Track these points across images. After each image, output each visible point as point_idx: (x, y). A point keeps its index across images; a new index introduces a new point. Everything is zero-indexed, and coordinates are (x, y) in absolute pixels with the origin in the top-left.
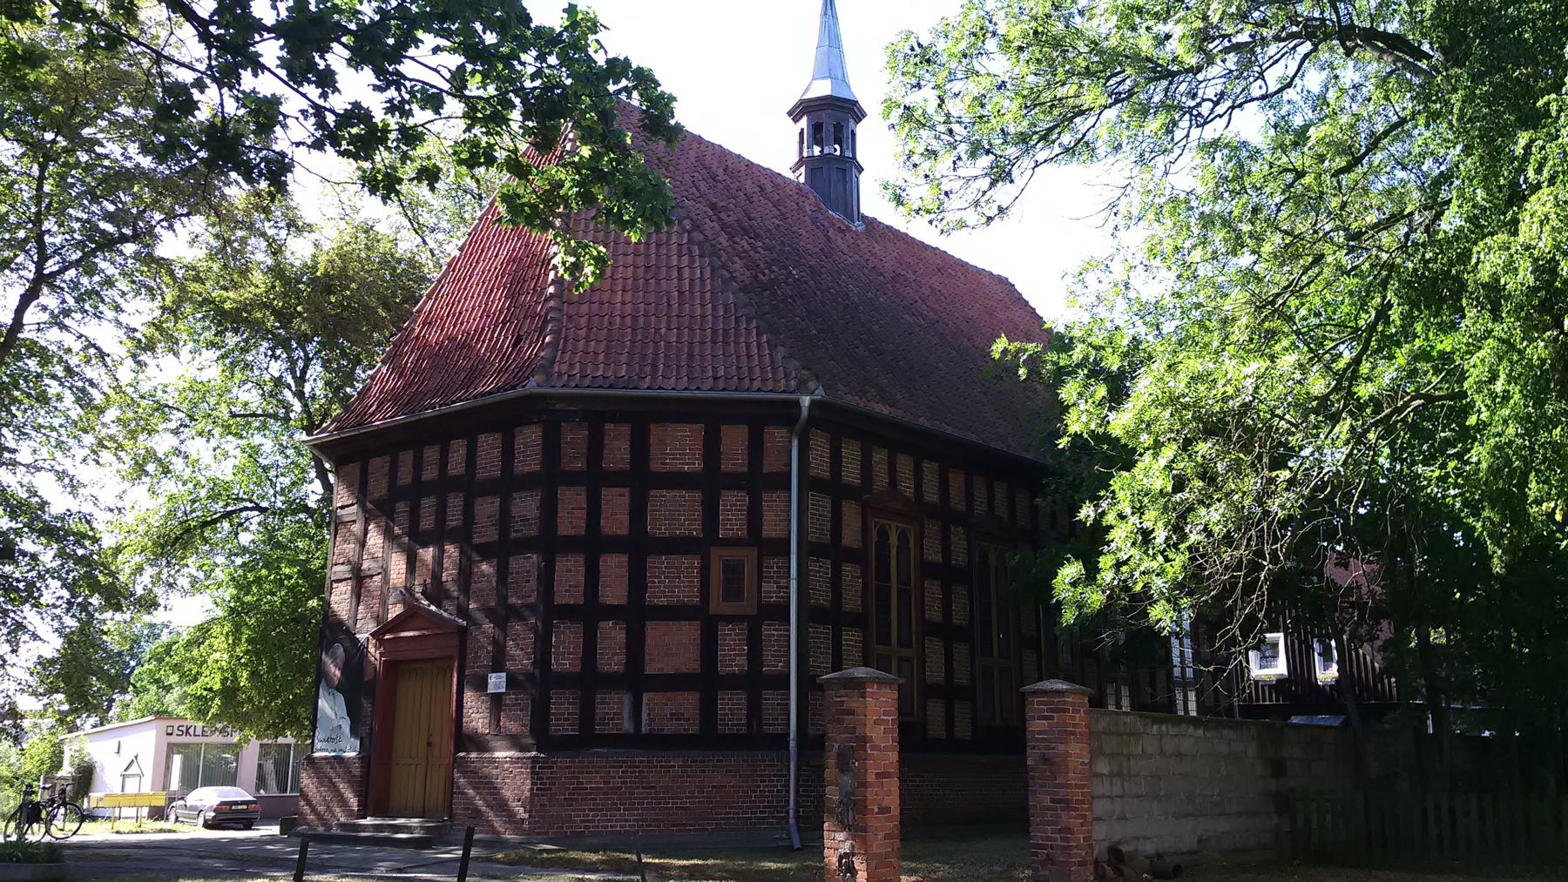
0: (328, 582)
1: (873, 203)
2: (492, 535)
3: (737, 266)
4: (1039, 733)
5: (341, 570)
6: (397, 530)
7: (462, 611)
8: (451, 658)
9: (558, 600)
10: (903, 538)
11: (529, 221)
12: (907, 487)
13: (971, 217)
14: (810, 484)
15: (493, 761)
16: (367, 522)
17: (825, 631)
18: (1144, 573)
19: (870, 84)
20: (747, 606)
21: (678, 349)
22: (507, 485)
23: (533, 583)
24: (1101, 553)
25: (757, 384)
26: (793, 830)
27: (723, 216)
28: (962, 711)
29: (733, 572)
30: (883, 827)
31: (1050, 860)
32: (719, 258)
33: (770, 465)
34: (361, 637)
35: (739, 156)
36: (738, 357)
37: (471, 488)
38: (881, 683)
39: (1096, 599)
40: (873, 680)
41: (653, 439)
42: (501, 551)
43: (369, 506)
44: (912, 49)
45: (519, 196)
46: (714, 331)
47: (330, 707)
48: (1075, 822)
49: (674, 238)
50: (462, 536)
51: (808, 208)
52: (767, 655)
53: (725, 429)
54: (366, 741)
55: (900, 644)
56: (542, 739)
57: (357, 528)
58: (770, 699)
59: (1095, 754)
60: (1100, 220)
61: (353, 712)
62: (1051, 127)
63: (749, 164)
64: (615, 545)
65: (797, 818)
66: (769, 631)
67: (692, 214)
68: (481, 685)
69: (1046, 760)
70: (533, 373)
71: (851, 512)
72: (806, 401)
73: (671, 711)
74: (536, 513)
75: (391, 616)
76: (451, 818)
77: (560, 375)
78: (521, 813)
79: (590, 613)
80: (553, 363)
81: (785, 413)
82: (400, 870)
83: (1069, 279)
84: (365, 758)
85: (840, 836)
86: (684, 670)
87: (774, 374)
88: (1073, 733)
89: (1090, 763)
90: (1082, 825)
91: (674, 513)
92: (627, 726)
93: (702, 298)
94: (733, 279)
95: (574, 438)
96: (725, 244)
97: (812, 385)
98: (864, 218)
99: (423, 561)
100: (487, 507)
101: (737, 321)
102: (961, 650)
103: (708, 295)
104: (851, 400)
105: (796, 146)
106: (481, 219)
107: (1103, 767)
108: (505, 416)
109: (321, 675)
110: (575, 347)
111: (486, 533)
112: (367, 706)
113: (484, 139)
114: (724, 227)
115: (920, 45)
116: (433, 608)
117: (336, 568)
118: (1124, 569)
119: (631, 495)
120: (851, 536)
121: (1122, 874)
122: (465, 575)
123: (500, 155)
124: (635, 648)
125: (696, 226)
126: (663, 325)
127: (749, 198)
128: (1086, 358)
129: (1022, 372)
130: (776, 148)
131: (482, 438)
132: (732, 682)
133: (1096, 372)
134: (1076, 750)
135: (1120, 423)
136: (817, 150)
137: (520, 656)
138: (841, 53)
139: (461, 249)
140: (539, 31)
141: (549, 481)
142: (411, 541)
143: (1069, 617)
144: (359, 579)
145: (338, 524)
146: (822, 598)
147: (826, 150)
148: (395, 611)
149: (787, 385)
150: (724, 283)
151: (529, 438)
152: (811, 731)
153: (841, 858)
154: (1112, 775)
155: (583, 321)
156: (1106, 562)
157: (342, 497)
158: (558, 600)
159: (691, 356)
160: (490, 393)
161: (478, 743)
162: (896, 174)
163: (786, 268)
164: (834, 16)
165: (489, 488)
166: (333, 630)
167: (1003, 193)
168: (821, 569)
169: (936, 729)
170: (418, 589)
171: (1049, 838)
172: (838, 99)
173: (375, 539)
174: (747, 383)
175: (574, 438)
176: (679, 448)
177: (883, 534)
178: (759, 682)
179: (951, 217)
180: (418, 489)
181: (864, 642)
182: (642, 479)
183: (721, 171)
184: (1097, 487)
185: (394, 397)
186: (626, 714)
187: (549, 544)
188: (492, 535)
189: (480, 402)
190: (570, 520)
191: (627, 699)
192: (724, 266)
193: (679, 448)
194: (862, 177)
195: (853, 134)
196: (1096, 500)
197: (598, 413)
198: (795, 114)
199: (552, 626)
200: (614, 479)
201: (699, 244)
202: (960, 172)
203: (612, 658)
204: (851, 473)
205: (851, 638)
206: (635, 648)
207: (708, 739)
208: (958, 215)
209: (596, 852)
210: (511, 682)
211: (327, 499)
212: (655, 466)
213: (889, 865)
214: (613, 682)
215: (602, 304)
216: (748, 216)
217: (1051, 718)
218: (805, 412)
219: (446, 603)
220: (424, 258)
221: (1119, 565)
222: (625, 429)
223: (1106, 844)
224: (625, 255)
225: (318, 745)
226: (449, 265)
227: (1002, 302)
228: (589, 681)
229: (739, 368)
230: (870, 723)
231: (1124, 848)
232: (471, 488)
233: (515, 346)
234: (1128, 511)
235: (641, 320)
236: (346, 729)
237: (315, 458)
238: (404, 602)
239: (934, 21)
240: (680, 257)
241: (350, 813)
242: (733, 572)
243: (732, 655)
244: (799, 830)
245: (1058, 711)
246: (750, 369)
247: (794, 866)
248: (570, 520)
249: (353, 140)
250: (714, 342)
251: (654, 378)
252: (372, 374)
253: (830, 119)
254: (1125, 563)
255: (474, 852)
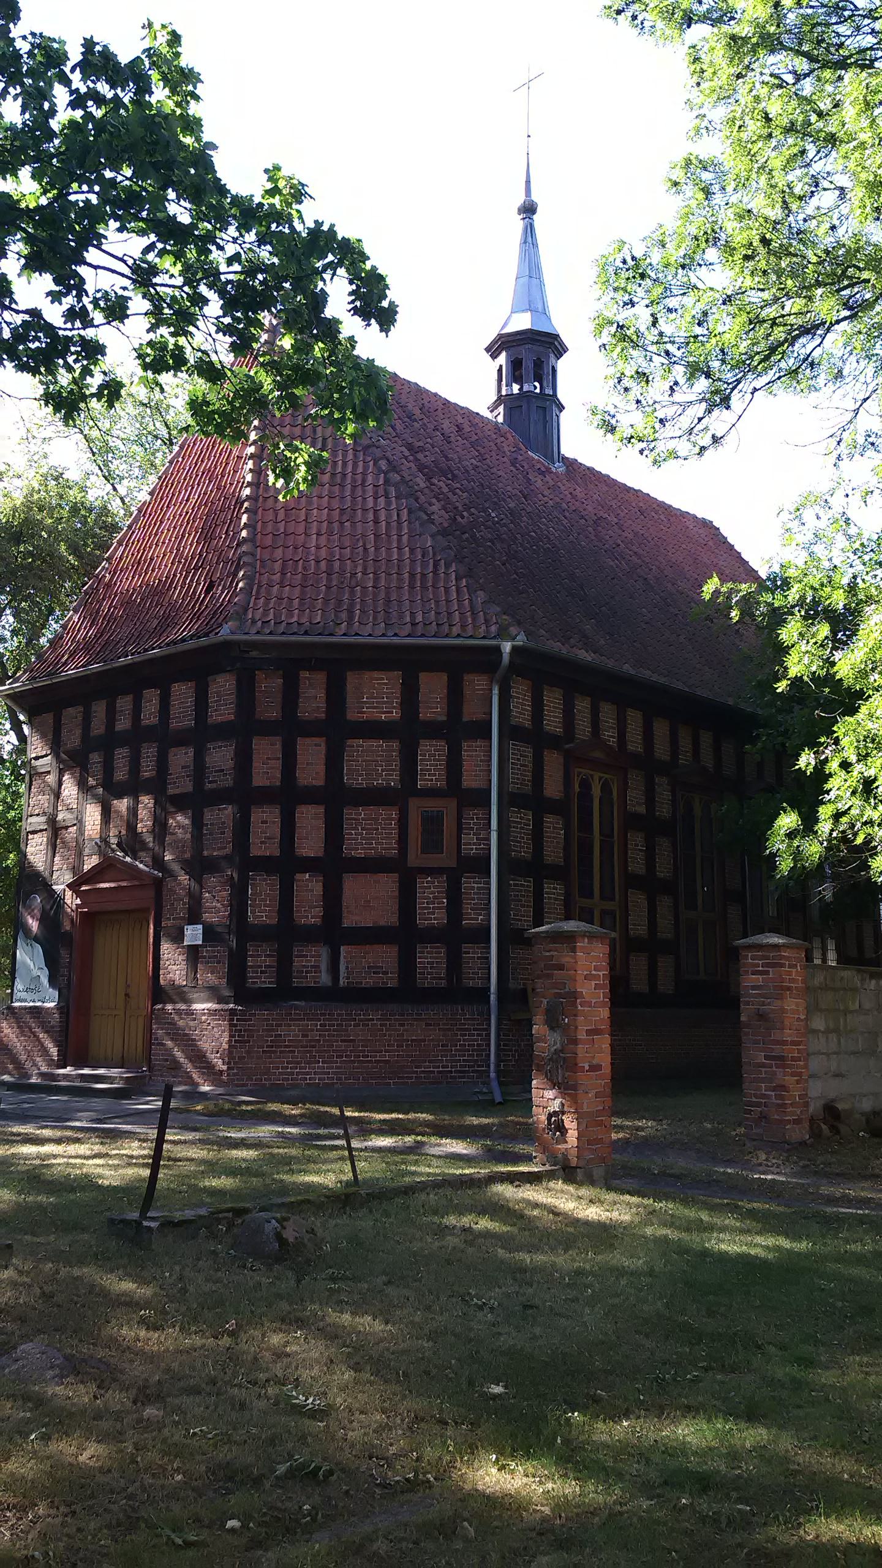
0: (23, 833)
1: (579, 440)
2: (187, 786)
3: (434, 508)
4: (754, 988)
5: (37, 822)
6: (91, 781)
7: (158, 862)
8: (146, 910)
9: (255, 852)
10: (606, 788)
11: (220, 430)
12: (610, 735)
13: (684, 447)
14: (509, 732)
15: (190, 1013)
16: (61, 773)
17: (526, 884)
18: (865, 823)
19: (575, 311)
20: (445, 859)
21: (375, 595)
22: (201, 735)
23: (229, 834)
24: (822, 803)
25: (456, 630)
26: (494, 1084)
27: (420, 456)
28: (666, 964)
29: (433, 823)
30: (595, 1087)
31: (763, 1117)
32: (417, 500)
33: (470, 712)
34: (58, 888)
35: (436, 395)
36: (437, 602)
37: (167, 738)
38: (592, 937)
39: (814, 849)
40: (584, 934)
41: (349, 687)
42: (195, 802)
43: (64, 756)
44: (624, 262)
45: (208, 404)
46: (412, 576)
47: (30, 959)
48: (789, 1080)
49: (370, 479)
50: (157, 787)
51: (506, 449)
52: (467, 909)
53: (423, 677)
54: (65, 991)
55: (603, 897)
56: (240, 992)
57: (51, 779)
58: (470, 952)
59: (812, 1009)
60: (821, 448)
61: (51, 962)
62: (775, 351)
63: (446, 403)
64: (310, 796)
65: (498, 1072)
66: (470, 884)
67: (388, 454)
68: (178, 937)
69: (761, 1016)
70: (226, 620)
71: (553, 763)
72: (507, 647)
73: (373, 965)
74: (231, 763)
75: (86, 868)
76: (150, 1069)
77: (254, 622)
78: (220, 1065)
79: (286, 865)
80: (246, 610)
81: (484, 659)
82: (99, 1121)
83: (785, 516)
84: (62, 1008)
85: (550, 1094)
86: (382, 923)
87: (474, 620)
88: (789, 989)
89: (806, 1019)
90: (798, 1082)
91: (372, 763)
92: (325, 979)
93: (399, 541)
94: (432, 522)
95: (269, 685)
96: (423, 485)
97: (513, 630)
98: (565, 460)
99: (117, 812)
100: (181, 758)
101: (436, 565)
102: (665, 903)
103: (405, 538)
104: (555, 647)
105: (494, 384)
106: (171, 462)
107: (818, 1023)
108: (197, 665)
109: (19, 926)
110: (268, 593)
111: (180, 784)
112: (64, 953)
113: (172, 340)
114: (421, 468)
115: (633, 258)
116: (128, 859)
117: (30, 820)
118: (844, 820)
119: (327, 743)
120: (553, 788)
121: (838, 1132)
122: (160, 827)
123: (191, 357)
124: (332, 900)
125: (393, 467)
126: (360, 569)
127: (447, 439)
128: (803, 598)
129: (735, 614)
130: (472, 385)
131: (175, 687)
132: (431, 936)
133: (815, 611)
134: (793, 1005)
135: (847, 665)
136: (516, 388)
137: (216, 906)
138: (541, 284)
139: (151, 494)
140: (237, 201)
141: (244, 729)
142: (107, 790)
143: (785, 865)
144: (55, 829)
145: (35, 774)
146: (523, 850)
147: (526, 388)
148: (91, 862)
149: (488, 631)
150: (421, 525)
151: (223, 686)
152: (512, 985)
153: (550, 1116)
154: (828, 1031)
155: (277, 566)
156: (825, 812)
157: (37, 747)
158: (255, 852)
159: (388, 601)
160: (183, 640)
161: (180, 994)
162: (607, 398)
163: (485, 510)
164: (535, 245)
165: (181, 739)
166: (32, 882)
167: (719, 422)
168: (523, 819)
169: (639, 984)
170: (114, 841)
171: (764, 1096)
172: (539, 333)
173: (70, 789)
174: (446, 628)
175: (269, 685)
176: (376, 696)
177: (586, 785)
178: (458, 936)
179: (661, 447)
180: (109, 743)
181: (568, 895)
182: (338, 729)
183: (417, 412)
184: (817, 732)
185: (86, 647)
186: (324, 967)
187: (244, 795)
188: (187, 786)
189: (172, 650)
190: (266, 769)
191: (324, 952)
192: (421, 508)
193: (376, 696)
194: (564, 416)
195: (554, 370)
196: (814, 745)
197: (293, 660)
198: (493, 350)
199: (248, 878)
200: (310, 729)
201: (396, 485)
202: (678, 397)
203: (309, 910)
204: (553, 722)
205: (553, 891)
206: (332, 900)
207: (407, 993)
208: (671, 445)
209: (294, 1103)
210: (209, 933)
211: (21, 750)
212: (352, 715)
213: (600, 1124)
214: (309, 935)
215: (296, 548)
216: (446, 457)
217: (767, 973)
218: (506, 658)
219: (142, 854)
220: (116, 506)
221: (837, 816)
222: (321, 677)
223: (823, 1102)
224: (320, 497)
225: (18, 995)
226: (140, 510)
227: (708, 545)
228: (286, 934)
229: (438, 613)
230: (580, 979)
231: (840, 1106)
232: (167, 738)
233: (207, 593)
234: (853, 758)
235: (337, 564)
236: (45, 981)
237: (10, 710)
238: (100, 852)
239: (647, 228)
240: (376, 499)
241: (50, 1063)
242: (433, 823)
243: (431, 909)
244: (500, 1084)
245: (774, 965)
246: (449, 614)
247: (496, 1121)
248: (266, 769)
249: (34, 354)
250: (412, 587)
251: (350, 624)
252: (63, 624)
253: (530, 355)
254: (845, 813)
255: (173, 1104)
